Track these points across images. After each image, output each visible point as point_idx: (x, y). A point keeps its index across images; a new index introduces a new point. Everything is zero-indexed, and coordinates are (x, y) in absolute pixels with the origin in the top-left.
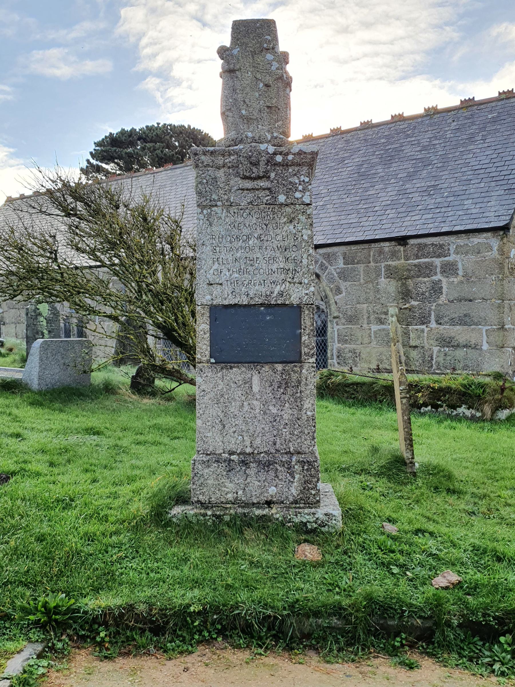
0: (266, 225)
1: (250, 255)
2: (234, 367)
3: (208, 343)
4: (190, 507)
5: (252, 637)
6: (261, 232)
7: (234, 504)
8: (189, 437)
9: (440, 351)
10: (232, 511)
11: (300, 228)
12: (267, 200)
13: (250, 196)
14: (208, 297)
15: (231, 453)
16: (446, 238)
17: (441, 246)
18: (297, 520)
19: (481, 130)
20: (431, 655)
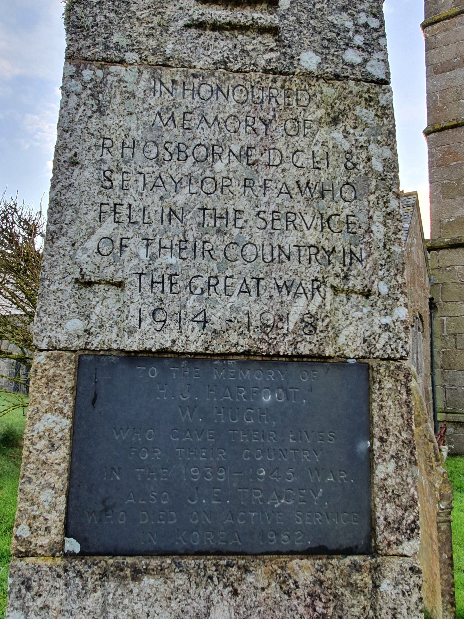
1: (216, 202)
2: (147, 571)
3: (60, 483)
6: (251, 140)
11: (362, 139)
12: (269, 61)
13: (222, 46)
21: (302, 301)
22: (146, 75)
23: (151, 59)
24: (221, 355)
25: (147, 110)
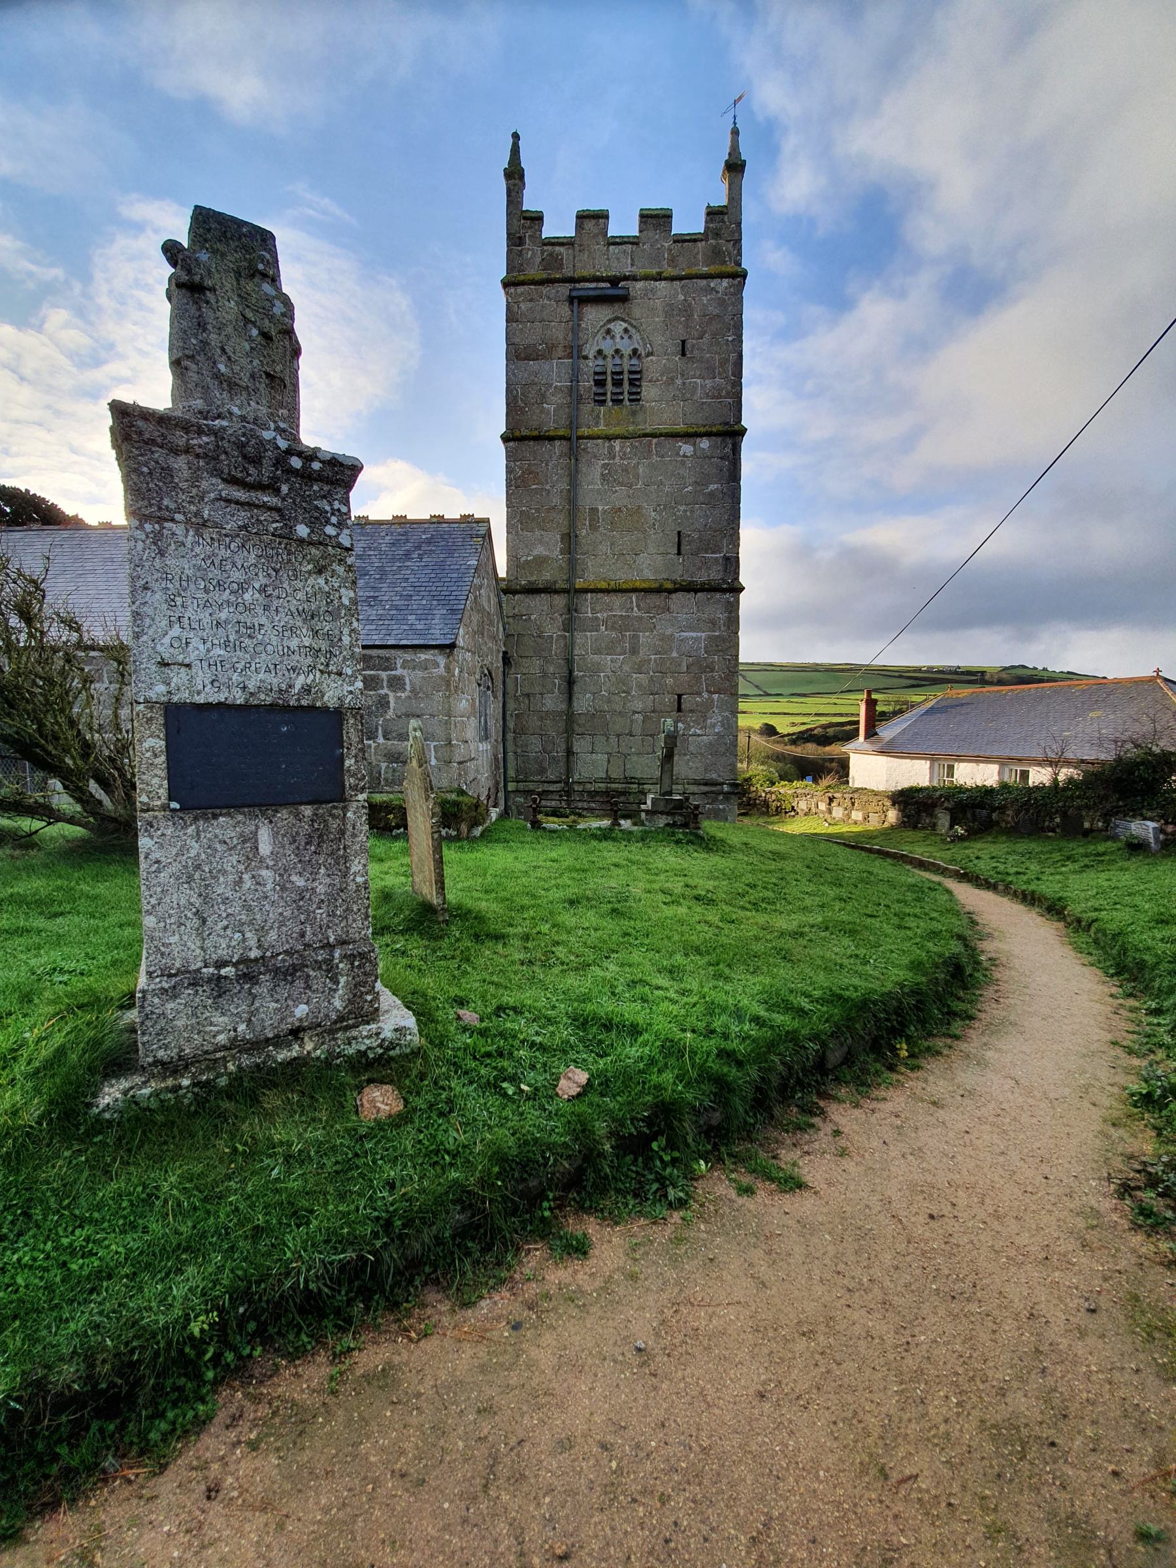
0: (277, 571)
2: (221, 815)
3: (164, 774)
4: (138, 1079)
5: (323, 1315)
7: (231, 1049)
8: (81, 909)
9: (388, 767)
10: (231, 1067)
11: (336, 585)
12: (276, 529)
13: (243, 516)
14: (161, 688)
15: (221, 964)
16: (393, 651)
17: (387, 659)
18: (350, 1051)
19: (419, 548)
20: (589, 1211)
21: (302, 677)
22: (191, 533)
23: (193, 520)
24: (255, 706)
25: (195, 556)
